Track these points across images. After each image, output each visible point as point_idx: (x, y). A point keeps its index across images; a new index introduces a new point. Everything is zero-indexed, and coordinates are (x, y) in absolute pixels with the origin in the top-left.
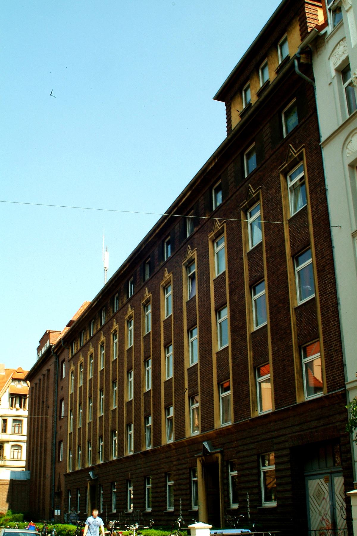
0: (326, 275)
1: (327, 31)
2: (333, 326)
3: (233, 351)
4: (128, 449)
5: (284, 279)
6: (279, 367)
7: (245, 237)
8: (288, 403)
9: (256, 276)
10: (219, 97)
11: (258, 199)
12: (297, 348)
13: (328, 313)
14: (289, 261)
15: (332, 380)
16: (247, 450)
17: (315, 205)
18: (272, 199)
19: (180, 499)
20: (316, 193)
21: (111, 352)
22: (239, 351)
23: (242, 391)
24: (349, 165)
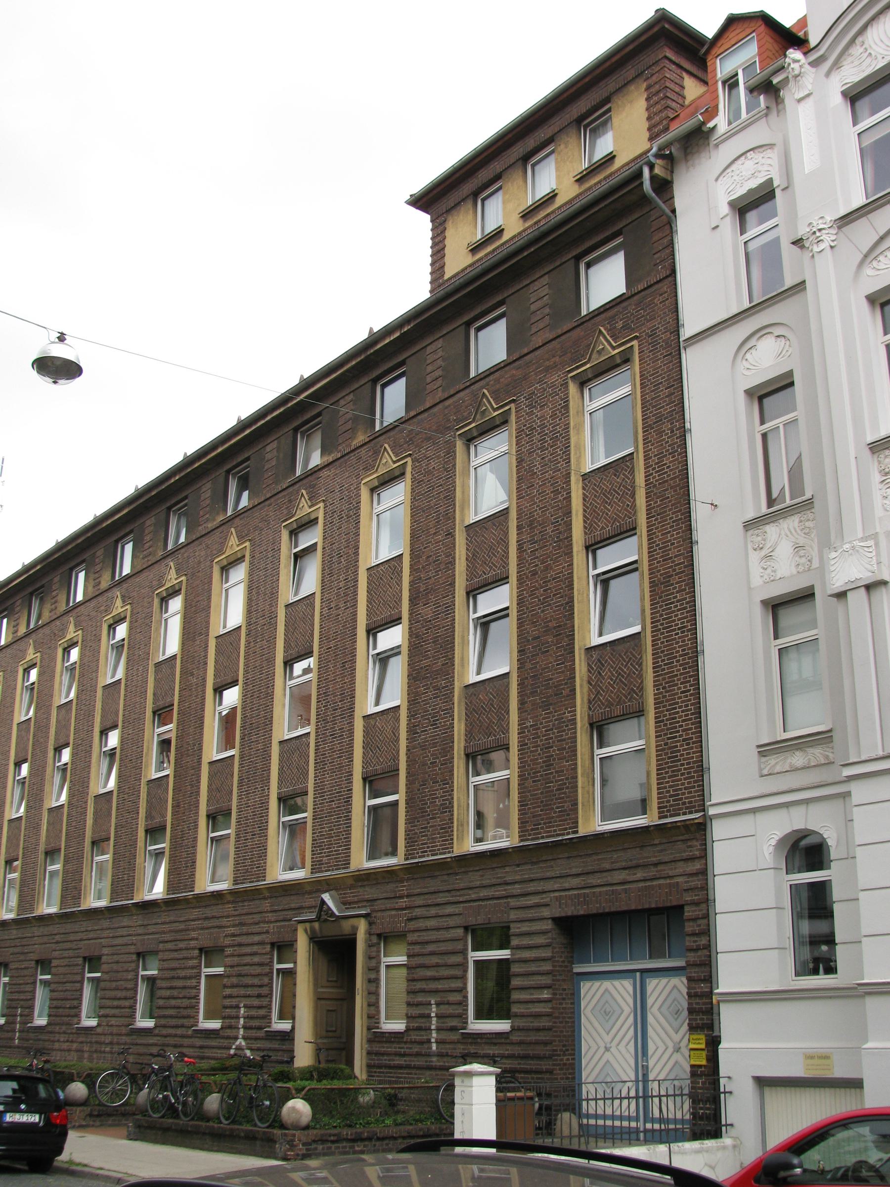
0: (673, 593)
1: (716, 125)
2: (682, 692)
3: (411, 715)
4: (90, 893)
5: (562, 588)
6: (537, 759)
7: (463, 492)
8: (555, 831)
9: (485, 574)
10: (422, 201)
11: (506, 422)
12: (585, 727)
13: (672, 667)
14: (577, 555)
15: (671, 796)
16: (437, 916)
17: (655, 456)
18: (543, 426)
19: (242, 1005)
20: (660, 433)
21: (56, 686)
22: (428, 719)
23: (433, 798)
24: (745, 391)
